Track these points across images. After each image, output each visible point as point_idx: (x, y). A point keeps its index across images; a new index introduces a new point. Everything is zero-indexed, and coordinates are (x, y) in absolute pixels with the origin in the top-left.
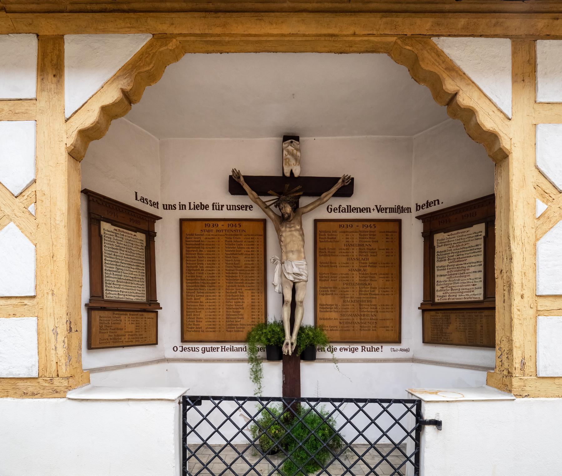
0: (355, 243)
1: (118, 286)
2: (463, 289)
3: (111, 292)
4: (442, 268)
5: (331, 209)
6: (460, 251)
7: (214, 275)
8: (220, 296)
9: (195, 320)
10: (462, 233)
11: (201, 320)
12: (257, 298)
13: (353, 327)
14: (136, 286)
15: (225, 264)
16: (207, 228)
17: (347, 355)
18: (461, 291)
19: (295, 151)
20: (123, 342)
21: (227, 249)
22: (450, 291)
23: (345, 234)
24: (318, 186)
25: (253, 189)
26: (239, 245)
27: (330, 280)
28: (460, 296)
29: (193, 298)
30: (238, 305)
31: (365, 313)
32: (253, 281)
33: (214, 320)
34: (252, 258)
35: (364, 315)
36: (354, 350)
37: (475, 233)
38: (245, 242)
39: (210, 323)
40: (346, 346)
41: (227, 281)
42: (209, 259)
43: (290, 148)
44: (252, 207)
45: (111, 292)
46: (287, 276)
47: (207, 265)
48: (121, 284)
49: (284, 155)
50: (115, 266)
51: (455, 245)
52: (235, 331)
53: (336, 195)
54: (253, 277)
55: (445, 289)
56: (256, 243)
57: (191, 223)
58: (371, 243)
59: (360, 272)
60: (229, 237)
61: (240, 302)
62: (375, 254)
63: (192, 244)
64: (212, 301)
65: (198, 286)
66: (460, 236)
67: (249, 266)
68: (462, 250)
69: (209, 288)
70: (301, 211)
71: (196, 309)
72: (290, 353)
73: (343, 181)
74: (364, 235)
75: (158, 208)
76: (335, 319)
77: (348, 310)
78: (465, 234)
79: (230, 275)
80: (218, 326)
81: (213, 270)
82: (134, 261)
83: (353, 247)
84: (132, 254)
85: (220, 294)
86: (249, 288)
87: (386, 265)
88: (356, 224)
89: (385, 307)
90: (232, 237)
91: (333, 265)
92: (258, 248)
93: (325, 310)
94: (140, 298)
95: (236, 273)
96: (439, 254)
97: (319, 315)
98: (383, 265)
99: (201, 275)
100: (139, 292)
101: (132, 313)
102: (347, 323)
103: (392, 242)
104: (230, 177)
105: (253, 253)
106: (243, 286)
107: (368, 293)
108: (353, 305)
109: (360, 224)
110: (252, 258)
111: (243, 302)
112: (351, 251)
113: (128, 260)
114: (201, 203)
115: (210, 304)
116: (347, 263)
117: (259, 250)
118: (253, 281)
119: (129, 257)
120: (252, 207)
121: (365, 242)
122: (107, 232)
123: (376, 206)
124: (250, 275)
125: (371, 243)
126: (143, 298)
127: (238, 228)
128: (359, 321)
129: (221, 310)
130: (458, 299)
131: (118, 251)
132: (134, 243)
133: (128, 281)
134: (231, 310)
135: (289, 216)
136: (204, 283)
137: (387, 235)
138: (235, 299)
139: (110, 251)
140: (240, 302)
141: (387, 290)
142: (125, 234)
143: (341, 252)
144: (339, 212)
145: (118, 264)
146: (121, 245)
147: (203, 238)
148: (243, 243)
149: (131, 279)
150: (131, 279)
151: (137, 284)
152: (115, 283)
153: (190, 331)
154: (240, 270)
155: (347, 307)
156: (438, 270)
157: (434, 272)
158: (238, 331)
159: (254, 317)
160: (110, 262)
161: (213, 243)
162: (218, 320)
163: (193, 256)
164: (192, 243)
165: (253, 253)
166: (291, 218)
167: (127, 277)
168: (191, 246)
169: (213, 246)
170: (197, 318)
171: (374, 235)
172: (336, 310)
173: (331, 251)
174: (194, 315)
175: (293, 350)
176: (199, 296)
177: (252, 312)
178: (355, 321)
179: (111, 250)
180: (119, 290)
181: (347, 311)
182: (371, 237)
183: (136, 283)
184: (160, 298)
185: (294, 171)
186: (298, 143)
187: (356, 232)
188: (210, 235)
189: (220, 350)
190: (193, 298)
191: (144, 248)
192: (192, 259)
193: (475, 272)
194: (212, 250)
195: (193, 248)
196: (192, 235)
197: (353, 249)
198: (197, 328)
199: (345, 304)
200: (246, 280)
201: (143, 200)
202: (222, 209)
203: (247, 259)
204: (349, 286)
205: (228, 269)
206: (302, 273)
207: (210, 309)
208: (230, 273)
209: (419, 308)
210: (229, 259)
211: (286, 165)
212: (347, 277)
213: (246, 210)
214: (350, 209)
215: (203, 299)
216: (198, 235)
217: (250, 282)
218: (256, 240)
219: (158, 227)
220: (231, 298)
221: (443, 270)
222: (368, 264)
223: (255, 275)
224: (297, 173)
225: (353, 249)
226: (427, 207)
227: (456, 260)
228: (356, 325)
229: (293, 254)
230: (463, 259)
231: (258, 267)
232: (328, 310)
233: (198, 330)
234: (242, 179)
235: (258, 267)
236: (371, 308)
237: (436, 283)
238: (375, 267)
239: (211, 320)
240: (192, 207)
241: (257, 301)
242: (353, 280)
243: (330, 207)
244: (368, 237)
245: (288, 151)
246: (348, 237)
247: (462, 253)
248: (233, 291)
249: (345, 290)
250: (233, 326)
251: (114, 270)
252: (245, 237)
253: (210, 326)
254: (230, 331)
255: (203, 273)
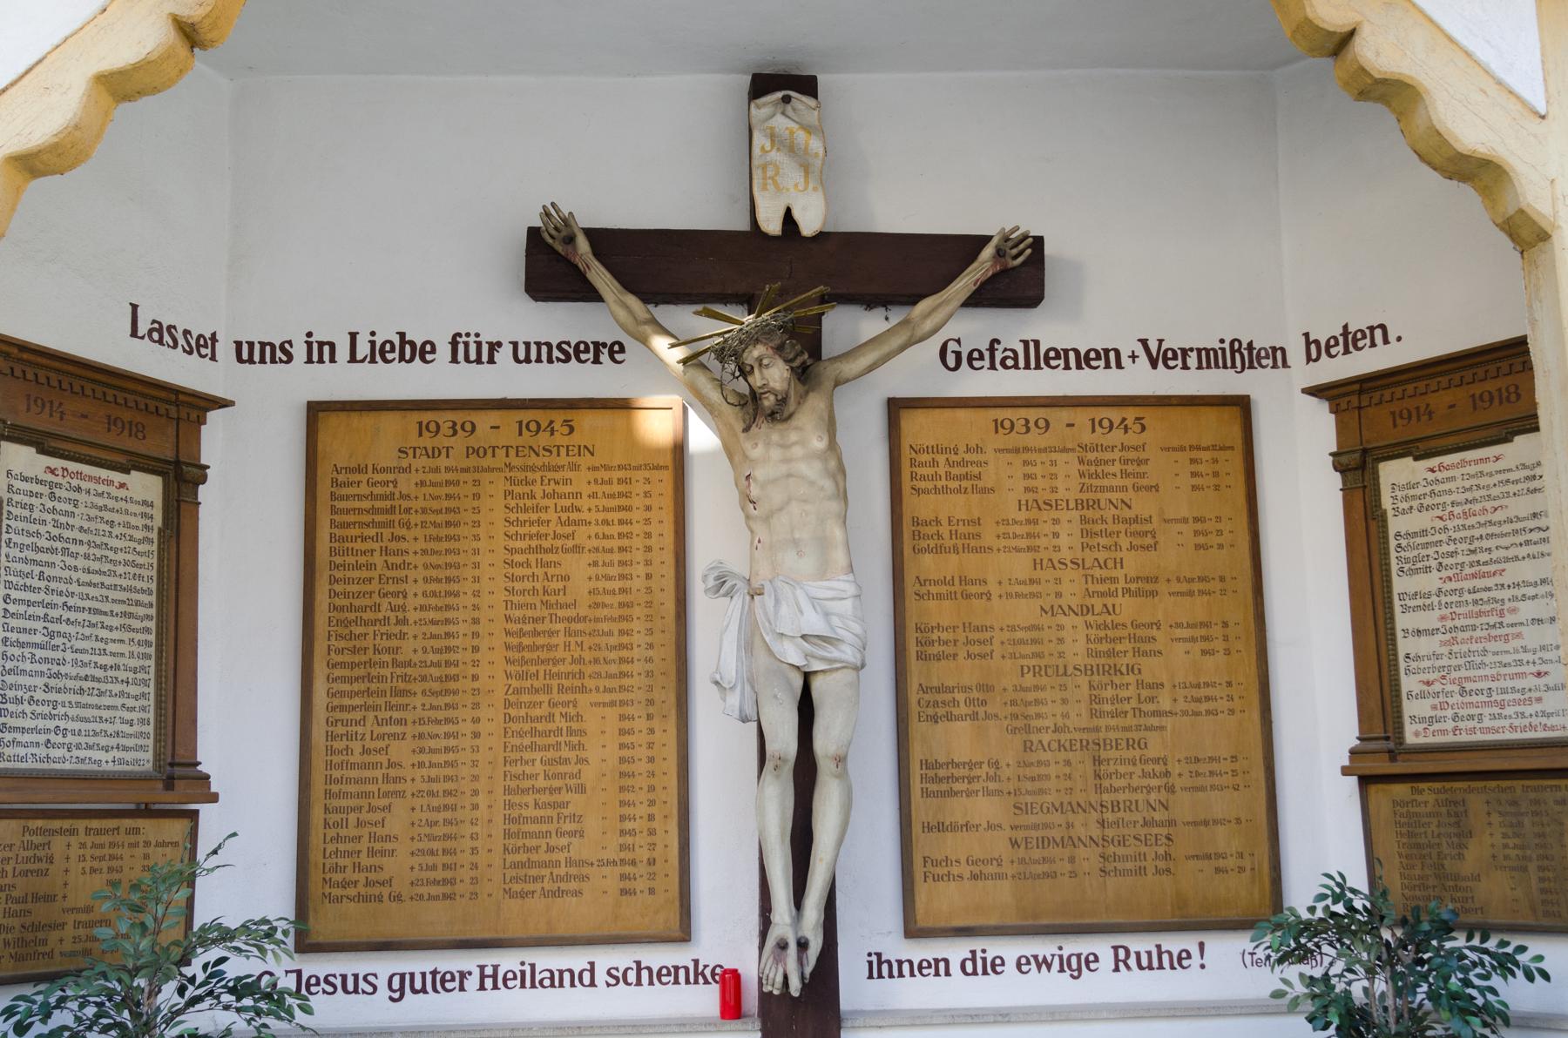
0: (1062, 494)
1: (46, 709)
2: (1504, 691)
3: (19, 737)
4: (1419, 602)
5: (958, 355)
6: (1476, 533)
7: (452, 642)
8: (476, 735)
9: (364, 845)
10: (1477, 462)
11: (388, 846)
12: (643, 738)
13: (1072, 860)
14: (118, 702)
15: (503, 596)
16: (427, 441)
17: (1053, 988)
18: (1495, 697)
19: (801, 135)
20: (50, 955)
21: (512, 530)
22: (1457, 699)
23: (1018, 460)
24: (899, 270)
25: (629, 283)
26: (566, 509)
27: (962, 654)
28: (1493, 717)
29: (356, 746)
30: (557, 776)
31: (1121, 797)
32: (625, 668)
33: (448, 844)
34: (622, 563)
35: (1115, 806)
36: (1079, 966)
37: (1524, 466)
38: (594, 495)
39: (430, 860)
40: (1044, 947)
41: (511, 669)
42: (434, 573)
43: (781, 123)
44: (622, 350)
45: (19, 737)
46: (776, 647)
47: (421, 600)
48: (60, 697)
49: (756, 151)
50: (39, 625)
51: (1457, 510)
52: (545, 894)
53: (978, 299)
54: (629, 647)
55: (1437, 687)
56: (637, 502)
57: (356, 420)
58: (1129, 496)
59: (1090, 618)
60: (520, 475)
61: (567, 761)
62: (1149, 541)
63: (360, 511)
64: (442, 758)
65: (383, 693)
66: (1472, 476)
67: (608, 599)
68: (1483, 531)
69: (428, 700)
70: (829, 372)
71: (367, 795)
72: (795, 987)
73: (1000, 253)
74: (1098, 462)
75: (213, 358)
76: (990, 827)
77: (1045, 785)
78: (1487, 467)
79: (526, 641)
80: (465, 874)
81: (447, 621)
82: (113, 595)
83: (1054, 514)
84: (106, 567)
85: (480, 727)
86: (607, 698)
87: (1196, 586)
88: (1065, 415)
89: (1204, 768)
90: (537, 476)
91: (973, 589)
92: (648, 521)
93: (944, 787)
94: (129, 756)
95: (551, 633)
96: (1404, 543)
97: (922, 810)
98: (1184, 587)
99: (394, 643)
100: (126, 728)
101: (95, 824)
102: (1043, 842)
103: (1217, 488)
104: (533, 233)
105: (625, 542)
106: (583, 689)
107: (1127, 707)
108: (1068, 763)
109: (1082, 416)
110: (622, 563)
111: (581, 761)
112: (1047, 528)
113: (93, 592)
114: (402, 335)
115: (434, 772)
116: (1032, 581)
117: (654, 529)
118: (625, 668)
119: (96, 579)
120: (622, 350)
121: (1103, 489)
122: (18, 484)
123: (1144, 342)
124: (613, 641)
125: (1129, 496)
126: (140, 755)
127: (559, 439)
128: (1096, 832)
129: (481, 800)
130: (1489, 730)
131: (57, 559)
132: (117, 518)
133: (86, 685)
134: (529, 799)
135: (783, 401)
136: (405, 678)
137: (1193, 461)
138: (547, 748)
139: (26, 561)
140: (567, 761)
141: (1209, 692)
142: (84, 485)
143: (1006, 536)
144: (993, 367)
145: (54, 613)
146: (67, 534)
147: (406, 484)
148: (584, 503)
149: (99, 673)
150: (99, 673)
151: (122, 694)
152: (39, 695)
153: (339, 899)
154: (569, 620)
155: (1043, 770)
156: (1406, 609)
157: (1391, 618)
158: (559, 893)
159: (629, 825)
160: (22, 609)
161: (452, 504)
162: (467, 844)
163: (362, 560)
164: (357, 504)
165: (625, 542)
166: (792, 406)
167: (84, 665)
168: (351, 518)
169: (451, 517)
170: (373, 837)
171: (1140, 462)
172: (992, 786)
173: (962, 529)
174: (359, 824)
175: (808, 970)
176: (381, 737)
177: (622, 803)
178: (1079, 831)
179: (31, 555)
180: (51, 724)
181: (1041, 792)
182: (1130, 468)
183: (116, 688)
184: (210, 755)
185: (796, 214)
186: (811, 102)
187: (1065, 450)
188: (437, 470)
189: (472, 982)
190: (356, 746)
191: (154, 535)
192: (356, 574)
193: (1540, 621)
194: (444, 532)
195: (362, 525)
196: (359, 470)
197: (1056, 521)
198: (368, 883)
199: (1033, 757)
200: (596, 661)
201: (161, 333)
202: (491, 361)
203: (601, 571)
204: (1044, 681)
205: (518, 613)
206: (842, 633)
207: (431, 794)
208: (522, 633)
209: (1346, 771)
210: (519, 572)
211: (764, 188)
212: (1034, 641)
213: (597, 361)
214: (1037, 356)
215: (400, 751)
216: (385, 470)
217: (613, 669)
218: (639, 488)
219: (216, 441)
220: (527, 741)
221: (1425, 608)
222: (1122, 584)
223: (636, 639)
224: (809, 225)
225: (1056, 521)
226: (1347, 352)
227: (1468, 570)
228: (1082, 852)
229: (800, 554)
230: (1493, 568)
231: (649, 604)
232: (957, 786)
233: (376, 891)
234: (583, 245)
235: (649, 604)
236: (1145, 775)
237: (1402, 665)
238: (1154, 594)
239: (435, 845)
240: (363, 349)
241: (643, 753)
242: (1061, 655)
243: (952, 346)
244: (1116, 468)
245: (773, 137)
246: (1029, 470)
247: (1485, 544)
248: (537, 712)
249: (1031, 696)
250: (533, 872)
251: (38, 638)
252: (591, 476)
253: (432, 875)
254: (523, 895)
255: (403, 636)
